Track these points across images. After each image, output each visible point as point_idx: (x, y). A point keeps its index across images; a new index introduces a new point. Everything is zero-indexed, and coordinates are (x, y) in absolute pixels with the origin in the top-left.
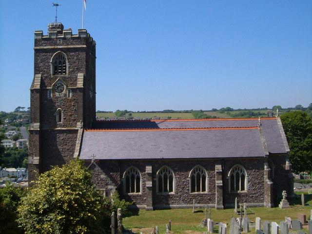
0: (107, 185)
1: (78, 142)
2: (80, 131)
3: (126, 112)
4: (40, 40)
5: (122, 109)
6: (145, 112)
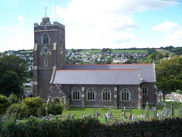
0: (62, 96)
1: (53, 76)
2: (54, 71)
3: (108, 49)
4: (37, 28)
5: (106, 47)
6: (119, 49)
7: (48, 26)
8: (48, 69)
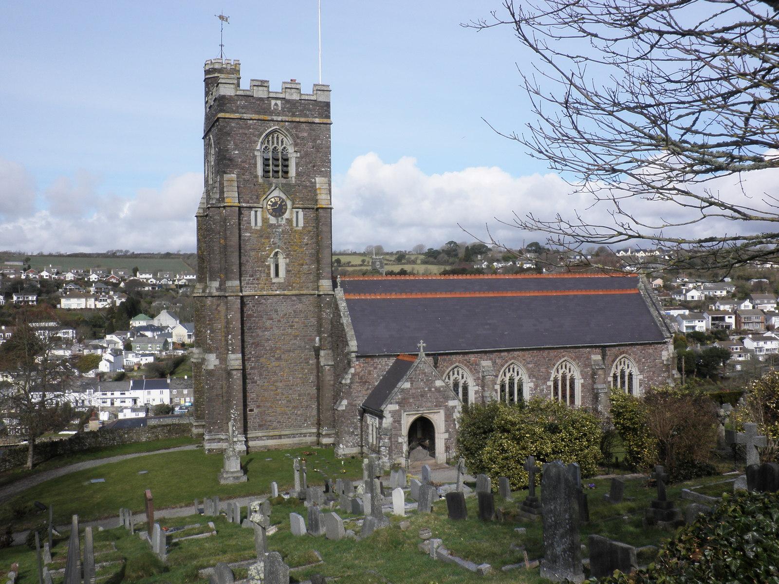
7: (288, 97)
8: (286, 292)
